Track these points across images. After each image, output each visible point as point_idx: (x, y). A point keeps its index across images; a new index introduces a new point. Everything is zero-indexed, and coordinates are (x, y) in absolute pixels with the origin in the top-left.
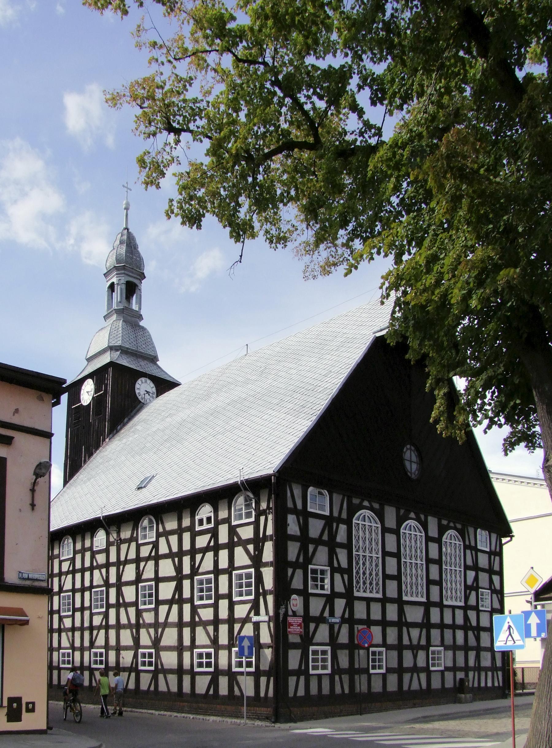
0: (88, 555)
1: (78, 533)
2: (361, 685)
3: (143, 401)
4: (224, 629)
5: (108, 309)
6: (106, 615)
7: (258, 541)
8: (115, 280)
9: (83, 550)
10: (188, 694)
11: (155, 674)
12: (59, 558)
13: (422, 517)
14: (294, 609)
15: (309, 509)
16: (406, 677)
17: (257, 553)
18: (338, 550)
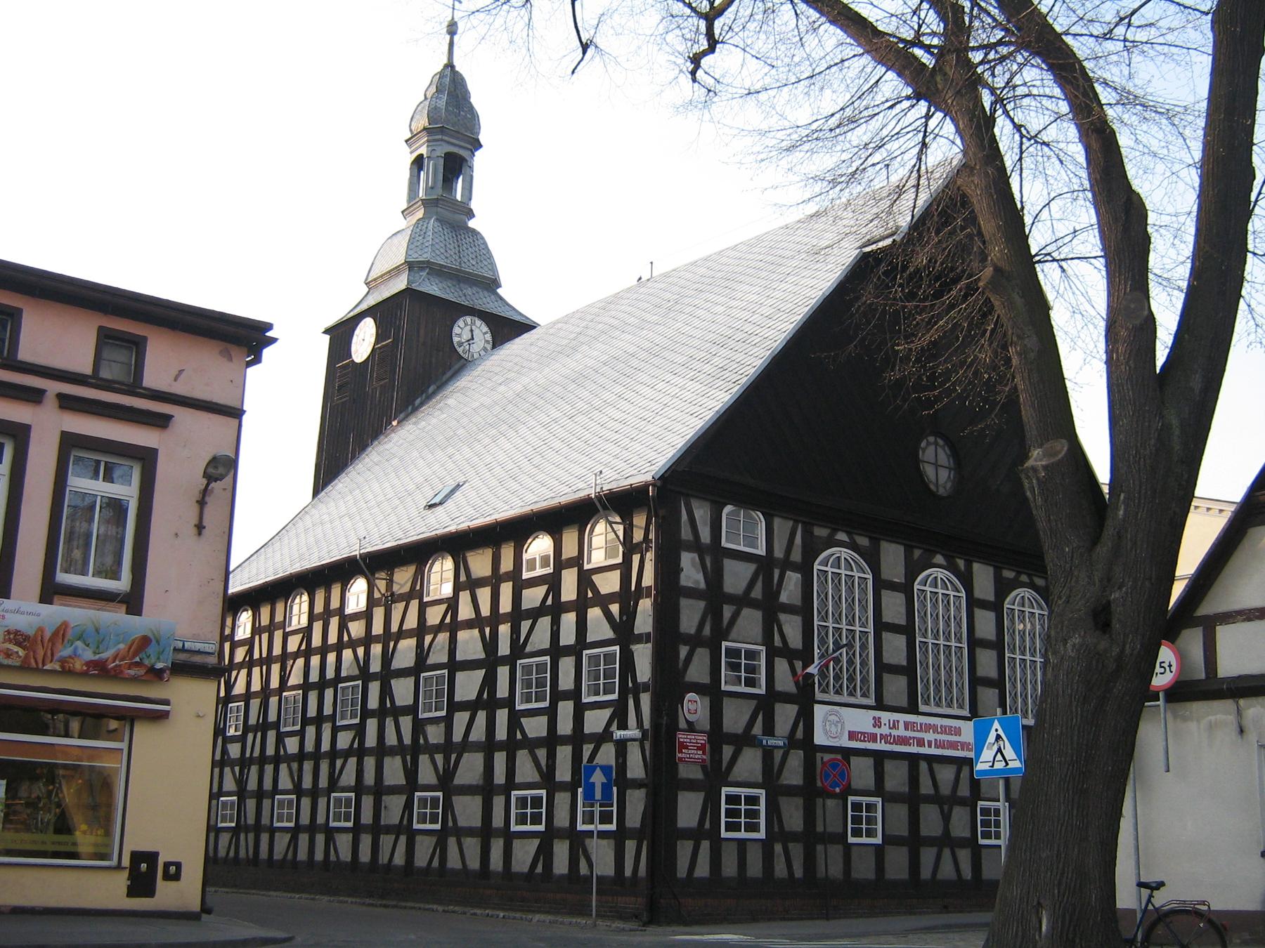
0: (334, 622)
1: (318, 586)
2: (830, 864)
3: (466, 356)
4: (564, 754)
5: (409, 201)
6: (360, 730)
7: (628, 597)
8: (423, 150)
10: (498, 873)
11: (441, 838)
13: (961, 563)
14: (690, 718)
18: (783, 617)
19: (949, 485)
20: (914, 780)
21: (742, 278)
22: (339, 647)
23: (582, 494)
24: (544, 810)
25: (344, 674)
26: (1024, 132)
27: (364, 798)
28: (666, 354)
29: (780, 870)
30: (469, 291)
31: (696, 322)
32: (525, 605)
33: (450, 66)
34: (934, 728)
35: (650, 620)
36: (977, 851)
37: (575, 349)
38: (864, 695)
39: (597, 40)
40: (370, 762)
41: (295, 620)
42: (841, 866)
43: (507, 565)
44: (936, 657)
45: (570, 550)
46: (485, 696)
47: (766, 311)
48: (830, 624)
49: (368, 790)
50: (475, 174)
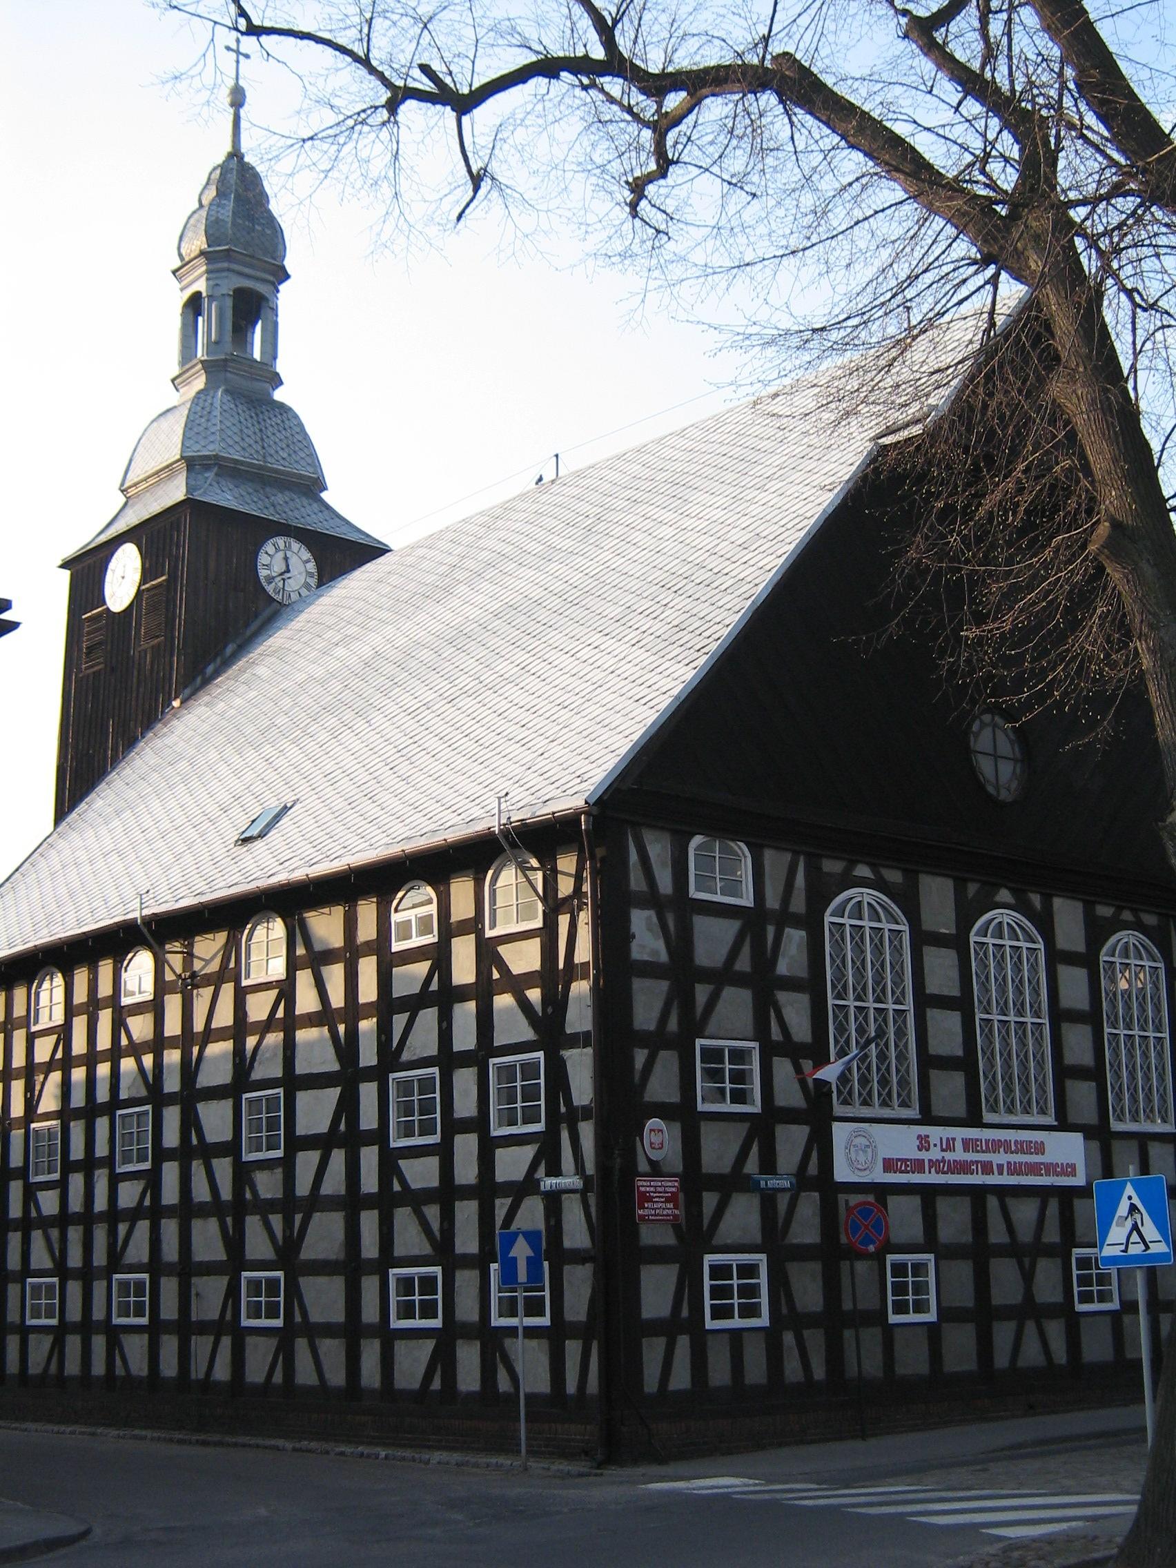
0: (105, 1017)
3: (278, 598)
4: (467, 1211)
6: (153, 1180)
7: (553, 977)
8: (201, 286)
9: (93, 1005)
10: (373, 1391)
11: (285, 1339)
12: (28, 1027)
13: (1036, 899)
14: (654, 1155)
15: (694, 893)
16: (1003, 1333)
17: (550, 1010)
18: (782, 997)
19: (1014, 785)
20: (979, 1223)
21: (697, 482)
22: (115, 1054)
23: (479, 827)
24: (439, 1297)
25: (124, 1095)
26: (1138, 299)
27: (163, 1280)
28: (590, 601)
29: (792, 1369)
30: (280, 498)
31: (633, 553)
32: (398, 991)
33: (236, 154)
34: (1005, 1146)
35: (589, 1013)
36: (1074, 1323)
37: (448, 590)
38: (904, 1104)
39: (494, 167)
40: (170, 1228)
41: (43, 1015)
42: (880, 1356)
43: (367, 930)
44: (1005, 1041)
45: (462, 907)
46: (342, 1127)
47: (739, 536)
48: (851, 1003)
49: (170, 1269)
50: (279, 319)
